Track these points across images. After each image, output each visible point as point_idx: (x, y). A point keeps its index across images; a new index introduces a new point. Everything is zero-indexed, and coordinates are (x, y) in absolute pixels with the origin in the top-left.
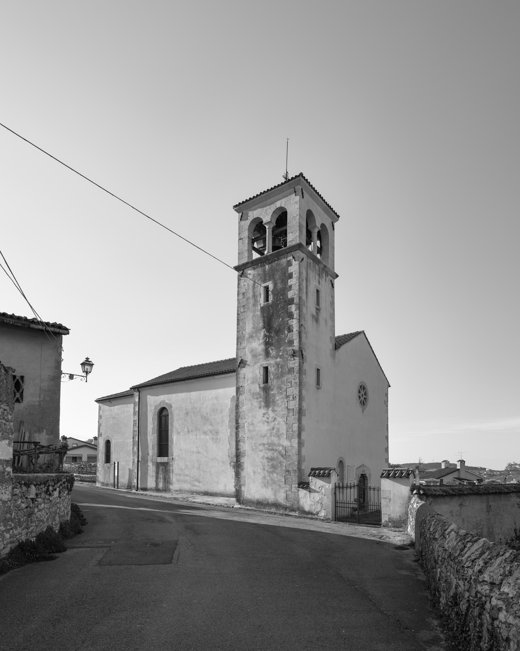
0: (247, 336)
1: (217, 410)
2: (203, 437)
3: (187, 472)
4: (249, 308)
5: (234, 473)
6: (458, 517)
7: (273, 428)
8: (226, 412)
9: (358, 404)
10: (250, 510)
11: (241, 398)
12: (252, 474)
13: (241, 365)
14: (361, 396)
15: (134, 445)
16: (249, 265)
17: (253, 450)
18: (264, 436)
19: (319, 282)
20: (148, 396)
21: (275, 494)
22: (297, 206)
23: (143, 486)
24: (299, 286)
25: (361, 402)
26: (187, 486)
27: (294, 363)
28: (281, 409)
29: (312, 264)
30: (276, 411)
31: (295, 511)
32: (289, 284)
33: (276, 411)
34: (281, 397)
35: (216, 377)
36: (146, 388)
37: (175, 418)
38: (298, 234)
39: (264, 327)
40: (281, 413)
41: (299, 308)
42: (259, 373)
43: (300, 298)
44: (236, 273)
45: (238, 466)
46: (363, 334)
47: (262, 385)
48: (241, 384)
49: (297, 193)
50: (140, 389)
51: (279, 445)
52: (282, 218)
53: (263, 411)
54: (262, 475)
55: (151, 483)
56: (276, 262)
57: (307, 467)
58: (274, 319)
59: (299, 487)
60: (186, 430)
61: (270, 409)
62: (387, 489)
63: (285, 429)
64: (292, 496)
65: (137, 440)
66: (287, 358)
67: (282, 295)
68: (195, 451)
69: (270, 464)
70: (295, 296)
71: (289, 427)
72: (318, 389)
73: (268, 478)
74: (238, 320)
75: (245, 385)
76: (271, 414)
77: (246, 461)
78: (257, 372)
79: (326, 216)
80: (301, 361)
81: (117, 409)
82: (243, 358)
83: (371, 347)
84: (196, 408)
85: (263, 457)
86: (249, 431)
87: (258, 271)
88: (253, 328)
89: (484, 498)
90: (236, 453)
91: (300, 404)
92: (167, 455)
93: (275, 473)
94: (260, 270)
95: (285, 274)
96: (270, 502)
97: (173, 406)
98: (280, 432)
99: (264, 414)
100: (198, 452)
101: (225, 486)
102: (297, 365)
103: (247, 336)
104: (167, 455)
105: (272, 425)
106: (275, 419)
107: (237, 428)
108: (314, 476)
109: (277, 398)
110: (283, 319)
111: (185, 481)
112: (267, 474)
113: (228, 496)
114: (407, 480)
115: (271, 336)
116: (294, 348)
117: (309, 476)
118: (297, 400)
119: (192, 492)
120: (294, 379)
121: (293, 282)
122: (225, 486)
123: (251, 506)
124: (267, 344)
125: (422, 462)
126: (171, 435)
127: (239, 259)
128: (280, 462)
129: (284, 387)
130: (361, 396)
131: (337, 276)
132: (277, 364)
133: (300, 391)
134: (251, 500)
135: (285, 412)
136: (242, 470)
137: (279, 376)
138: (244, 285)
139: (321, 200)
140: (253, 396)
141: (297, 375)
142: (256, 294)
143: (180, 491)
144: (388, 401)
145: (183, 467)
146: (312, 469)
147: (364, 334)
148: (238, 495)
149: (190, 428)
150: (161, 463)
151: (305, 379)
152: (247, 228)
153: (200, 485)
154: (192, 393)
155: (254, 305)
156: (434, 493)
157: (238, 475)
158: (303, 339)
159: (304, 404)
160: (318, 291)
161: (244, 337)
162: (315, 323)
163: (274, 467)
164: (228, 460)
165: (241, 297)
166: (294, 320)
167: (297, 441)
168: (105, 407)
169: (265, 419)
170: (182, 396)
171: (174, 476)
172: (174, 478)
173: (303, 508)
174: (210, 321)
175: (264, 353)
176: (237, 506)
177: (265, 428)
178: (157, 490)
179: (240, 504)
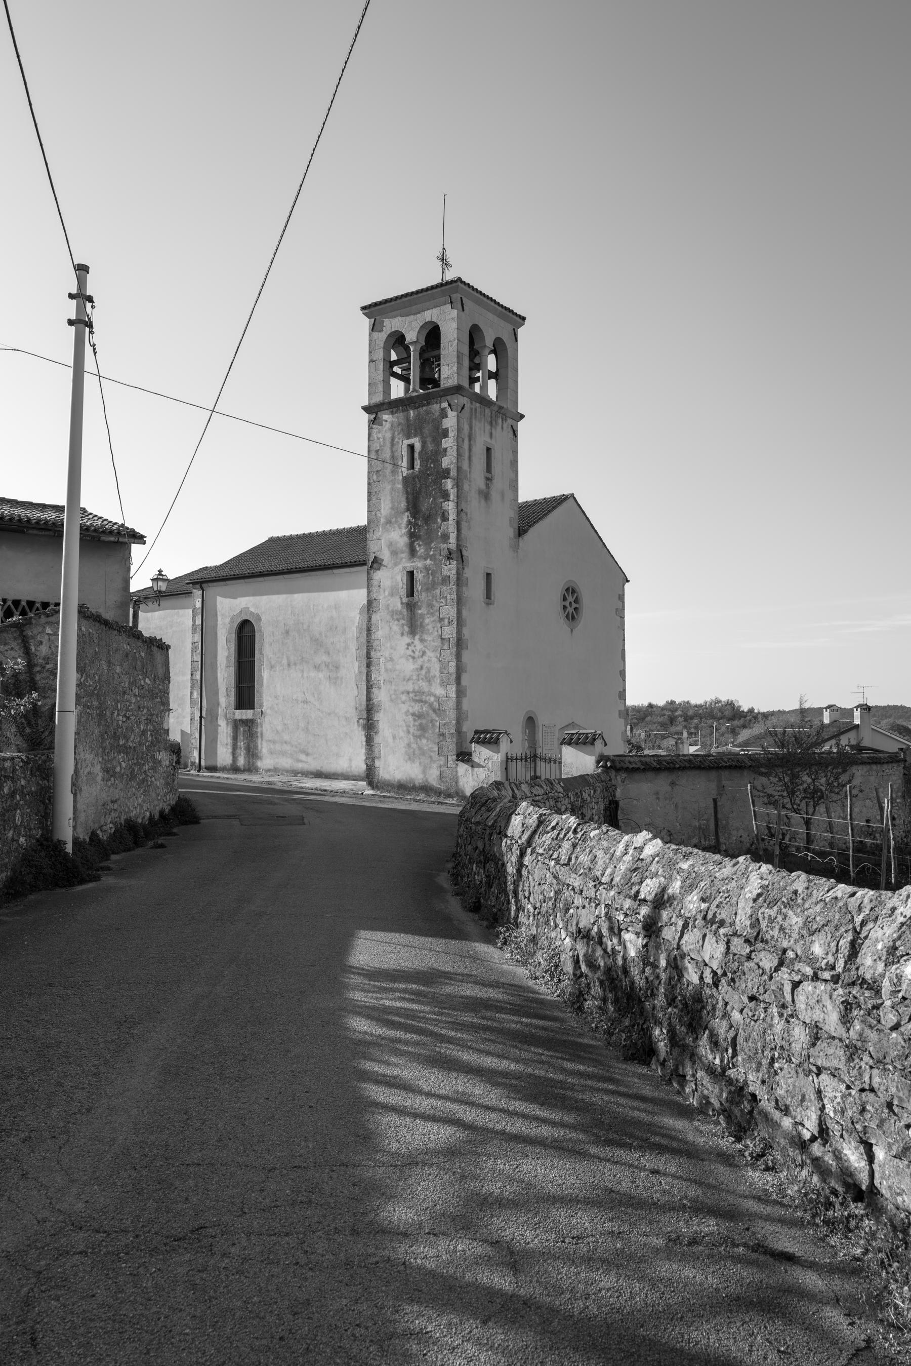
0: (382, 520)
1: (336, 628)
2: (313, 674)
3: (286, 737)
4: (385, 476)
5: (364, 739)
6: (668, 801)
7: (422, 668)
8: (352, 632)
9: (562, 621)
10: (389, 797)
11: (375, 617)
12: (390, 740)
13: (375, 565)
14: (568, 605)
15: (192, 687)
16: (385, 407)
17: (392, 700)
18: (408, 680)
19: (491, 434)
20: (219, 599)
21: (424, 772)
22: (455, 325)
23: (210, 763)
24: (458, 450)
25: (567, 617)
26: (286, 763)
27: (450, 570)
28: (432, 638)
29: (478, 410)
30: (426, 641)
31: (452, 797)
32: (444, 445)
33: (426, 641)
34: (432, 619)
35: (335, 571)
36: (215, 584)
37: (267, 639)
38: (455, 368)
39: (408, 510)
40: (433, 644)
41: (458, 485)
42: (401, 581)
43: (459, 469)
44: (365, 417)
45: (370, 727)
46: (572, 499)
47: (405, 600)
48: (374, 596)
49: (455, 304)
50: (204, 585)
51: (431, 694)
52: (433, 335)
53: (407, 639)
54: (406, 742)
55: (224, 756)
56: (425, 408)
57: (469, 728)
58: (422, 493)
59: (457, 760)
60: (285, 662)
61: (417, 637)
62: (569, 760)
63: (438, 669)
64: (448, 773)
65: (198, 677)
66: (440, 561)
67: (433, 462)
68: (300, 699)
69: (417, 723)
70: (452, 467)
71: (444, 667)
72: (488, 604)
73: (414, 746)
74: (370, 494)
75: (381, 597)
76: (419, 646)
77: (381, 718)
78: (399, 578)
79: (502, 323)
80: (461, 566)
81: (756, 803)
82: (378, 554)
83: (587, 518)
84: (303, 624)
85: (407, 713)
86: (386, 670)
87: (398, 418)
88: (392, 508)
89: (713, 774)
90: (367, 705)
91: (459, 632)
92: (251, 706)
93: (424, 737)
94: (400, 417)
95: (438, 429)
96: (417, 785)
97: (263, 618)
98: (432, 674)
99: (408, 645)
100: (306, 702)
101: (350, 760)
102: (454, 572)
103: (382, 520)
104: (251, 706)
105: (420, 662)
106: (424, 653)
107: (368, 665)
108: (478, 743)
109: (427, 621)
110: (435, 499)
111: (283, 753)
112: (412, 740)
113: (355, 778)
114: (591, 747)
115: (417, 524)
116: (450, 546)
117: (471, 742)
118: (455, 625)
119: (295, 773)
120: (450, 594)
121: (449, 443)
122: (350, 760)
123: (389, 792)
124: (413, 536)
125: (807, 706)
126: (260, 670)
127: (370, 399)
128: (432, 721)
129: (437, 605)
130: (568, 605)
131: (522, 416)
132: (427, 569)
133: (459, 612)
134: (389, 781)
135: (438, 643)
136: (376, 733)
137: (430, 588)
138: (378, 438)
139: (493, 304)
140: (392, 616)
141: (454, 587)
142: (396, 454)
143: (275, 771)
144: (623, 608)
145: (280, 728)
146: (476, 732)
147: (575, 498)
148: (370, 776)
149: (292, 659)
150: (241, 720)
151: (467, 592)
152: (382, 345)
153: (309, 759)
154: (296, 595)
155: (393, 472)
156: (628, 765)
157: (369, 741)
158: (464, 532)
159: (466, 631)
160: (488, 449)
161: (378, 521)
162: (483, 502)
163: (422, 728)
164: (353, 715)
165: (373, 456)
166: (450, 503)
167: (454, 689)
168: (361, 558)
169: (409, 652)
170: (278, 600)
171: (265, 744)
172: (264, 747)
173: (463, 792)
174: (329, 483)
175: (407, 550)
176: (369, 792)
177: (409, 667)
178: (235, 769)
179: (373, 789)
